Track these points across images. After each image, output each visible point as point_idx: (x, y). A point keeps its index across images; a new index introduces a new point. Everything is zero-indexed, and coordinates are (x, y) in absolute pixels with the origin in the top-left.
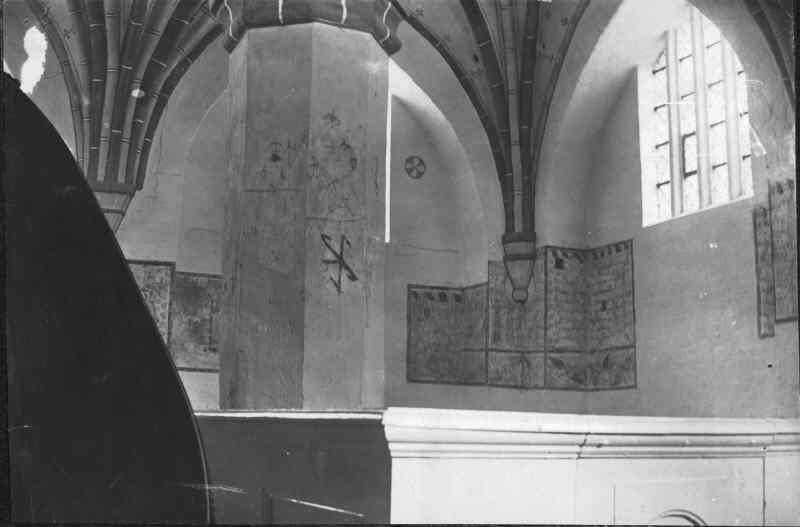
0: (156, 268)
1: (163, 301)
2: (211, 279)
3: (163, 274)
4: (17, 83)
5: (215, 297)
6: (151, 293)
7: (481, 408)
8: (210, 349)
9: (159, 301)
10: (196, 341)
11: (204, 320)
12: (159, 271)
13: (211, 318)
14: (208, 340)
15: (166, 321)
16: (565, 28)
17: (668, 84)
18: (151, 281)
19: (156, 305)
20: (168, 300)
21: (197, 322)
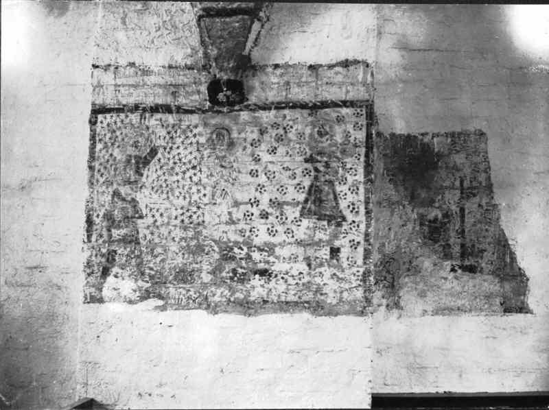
13: (462, 210)
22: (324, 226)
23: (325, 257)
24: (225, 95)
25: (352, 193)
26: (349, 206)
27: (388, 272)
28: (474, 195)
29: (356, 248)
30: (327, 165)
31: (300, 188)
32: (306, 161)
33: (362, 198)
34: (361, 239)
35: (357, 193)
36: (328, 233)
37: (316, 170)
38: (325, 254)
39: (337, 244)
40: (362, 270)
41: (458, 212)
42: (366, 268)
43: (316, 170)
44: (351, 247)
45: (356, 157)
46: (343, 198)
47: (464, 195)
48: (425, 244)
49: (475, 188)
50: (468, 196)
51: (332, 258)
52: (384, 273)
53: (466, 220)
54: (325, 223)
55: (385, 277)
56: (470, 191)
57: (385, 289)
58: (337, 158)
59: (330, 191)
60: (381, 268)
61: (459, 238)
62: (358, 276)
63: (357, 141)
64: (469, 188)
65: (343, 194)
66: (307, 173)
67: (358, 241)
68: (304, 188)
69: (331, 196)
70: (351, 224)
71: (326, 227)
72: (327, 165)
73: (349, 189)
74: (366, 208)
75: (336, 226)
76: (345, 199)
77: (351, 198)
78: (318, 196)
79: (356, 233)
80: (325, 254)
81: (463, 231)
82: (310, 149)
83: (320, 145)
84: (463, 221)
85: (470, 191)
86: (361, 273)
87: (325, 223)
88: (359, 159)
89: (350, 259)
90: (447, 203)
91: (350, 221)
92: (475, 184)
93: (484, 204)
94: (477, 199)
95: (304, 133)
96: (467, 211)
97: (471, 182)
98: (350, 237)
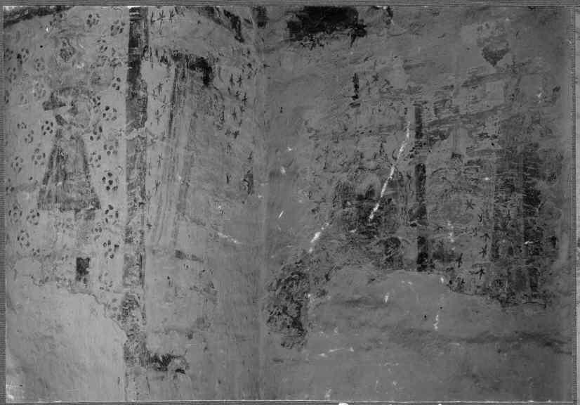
13: (421, 168)
22: (69, 220)
23: (68, 277)
24: (51, 37)
25: (109, 153)
26: (104, 179)
27: (290, 298)
28: (443, 137)
29: (112, 257)
30: (74, 111)
31: (39, 158)
32: (46, 107)
33: (122, 160)
34: (119, 239)
35: (115, 153)
36: (74, 233)
37: (59, 119)
38: (70, 272)
39: (86, 252)
40: (120, 297)
41: (412, 175)
42: (127, 294)
43: (59, 119)
44: (106, 254)
45: (114, 86)
46: (95, 165)
47: (423, 140)
48: (352, 241)
49: (445, 121)
50: (431, 140)
51: (78, 279)
52: (283, 302)
53: (427, 190)
54: (71, 214)
55: (285, 309)
56: (435, 128)
57: (286, 330)
58: (88, 93)
59: (79, 155)
60: (277, 292)
61: (414, 225)
62: (115, 309)
63: (116, 56)
64: (434, 123)
65: (95, 157)
66: (48, 129)
67: (116, 243)
68: (44, 155)
69: (81, 165)
70: (107, 211)
71: (73, 222)
72: (74, 111)
73: (105, 147)
74: (128, 179)
75: (86, 219)
76: (99, 166)
77: (106, 166)
78: (63, 167)
79: (113, 228)
80: (70, 272)
81: (422, 212)
82: (51, 86)
83: (65, 74)
84: (421, 193)
85: (435, 128)
86: (119, 303)
87: (71, 214)
88: (118, 88)
89: (103, 278)
90: (390, 157)
91: (105, 208)
92: (445, 114)
93: (463, 151)
94: (447, 144)
95: (42, 59)
96: (429, 171)
97: (436, 110)
98: (105, 236)
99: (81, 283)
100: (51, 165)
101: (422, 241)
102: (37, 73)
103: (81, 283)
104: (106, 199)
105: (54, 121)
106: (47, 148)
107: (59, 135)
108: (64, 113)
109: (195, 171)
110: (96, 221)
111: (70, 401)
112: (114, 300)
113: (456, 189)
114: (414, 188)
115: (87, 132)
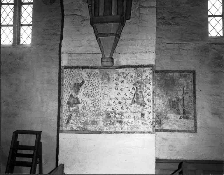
0: (142, 69)
1: (148, 91)
2: (182, 73)
3: (147, 74)
4: (14, 7)
5: (185, 85)
6: (140, 86)
7: (21, 157)
8: (184, 118)
9: (145, 91)
10: (175, 112)
11: (178, 100)
12: (144, 71)
13: (183, 98)
14: (182, 112)
15: (151, 104)
16: (64, 90)
17: (59, 118)
18: (139, 79)
19: (221, 63)
20: (151, 91)
21: (175, 101)
32: (134, 85)
37: (136, 88)
39: (143, 112)
51: (142, 117)
73: (147, 94)
81: (184, 105)
86: (151, 122)
96: (185, 99)
99: (143, 118)
100: (134, 95)
101: (184, 110)
102: (131, 78)
103: (143, 118)
104: (148, 103)
105: (135, 88)
106: (134, 92)
107: (137, 91)
108: (138, 87)
109: (116, 75)
110: (146, 107)
111: (21, 153)
112: (151, 121)
113: (190, 102)
114: (182, 101)
115: (143, 91)
